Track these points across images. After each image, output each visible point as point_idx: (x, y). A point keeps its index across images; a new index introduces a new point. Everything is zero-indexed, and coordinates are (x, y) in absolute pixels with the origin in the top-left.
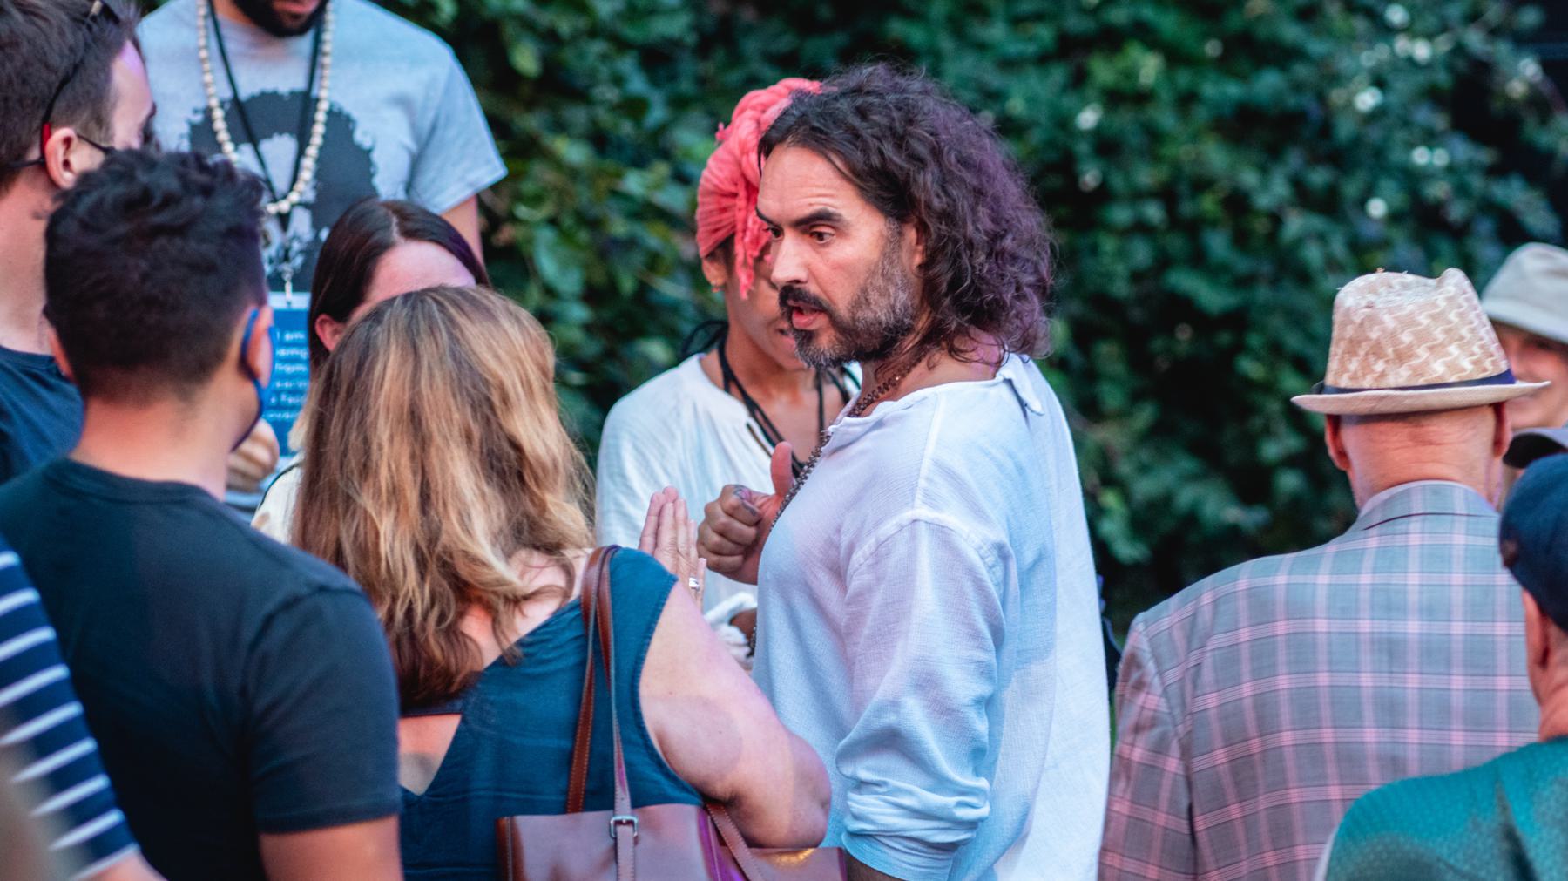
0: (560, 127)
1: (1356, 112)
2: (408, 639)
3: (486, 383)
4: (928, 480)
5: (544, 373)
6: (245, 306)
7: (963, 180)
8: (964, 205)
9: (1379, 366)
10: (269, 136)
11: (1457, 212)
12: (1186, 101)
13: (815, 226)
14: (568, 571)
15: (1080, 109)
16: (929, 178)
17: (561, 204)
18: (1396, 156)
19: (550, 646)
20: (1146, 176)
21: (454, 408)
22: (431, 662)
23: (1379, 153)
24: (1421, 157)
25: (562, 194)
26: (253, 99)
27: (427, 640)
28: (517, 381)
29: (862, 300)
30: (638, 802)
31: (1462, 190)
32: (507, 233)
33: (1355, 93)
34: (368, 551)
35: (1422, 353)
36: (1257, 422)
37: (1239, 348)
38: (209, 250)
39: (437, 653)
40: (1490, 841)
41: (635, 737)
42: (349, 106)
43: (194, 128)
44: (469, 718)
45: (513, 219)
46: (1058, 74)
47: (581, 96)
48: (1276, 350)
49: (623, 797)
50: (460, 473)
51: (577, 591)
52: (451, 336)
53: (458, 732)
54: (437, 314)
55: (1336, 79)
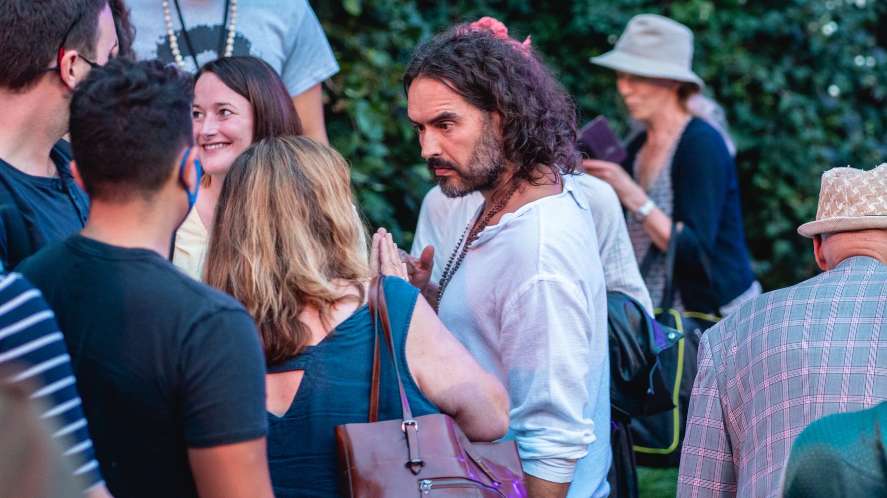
0: (371, 44)
1: (824, 36)
2: (270, 324)
3: (312, 184)
5: (345, 181)
6: (181, 149)
7: (520, 84)
8: (521, 98)
9: (840, 206)
10: (202, 52)
12: (726, 29)
14: (360, 287)
16: (500, 85)
17: (372, 88)
18: (845, 61)
19: (354, 330)
21: (294, 198)
22: (284, 339)
23: (836, 59)
24: (859, 61)
25: (372, 82)
26: (193, 30)
27: (282, 327)
28: (330, 187)
29: (475, 159)
30: (414, 415)
32: (341, 105)
33: (822, 25)
34: (245, 279)
35: (864, 199)
36: (765, 213)
37: (755, 170)
38: (163, 114)
39: (288, 334)
40: (870, 450)
41: (407, 380)
42: (247, 34)
43: (160, 47)
45: (345, 97)
47: (384, 26)
48: (776, 172)
49: (407, 414)
50: (299, 233)
51: (366, 300)
52: (292, 159)
54: (284, 148)
55: (812, 16)
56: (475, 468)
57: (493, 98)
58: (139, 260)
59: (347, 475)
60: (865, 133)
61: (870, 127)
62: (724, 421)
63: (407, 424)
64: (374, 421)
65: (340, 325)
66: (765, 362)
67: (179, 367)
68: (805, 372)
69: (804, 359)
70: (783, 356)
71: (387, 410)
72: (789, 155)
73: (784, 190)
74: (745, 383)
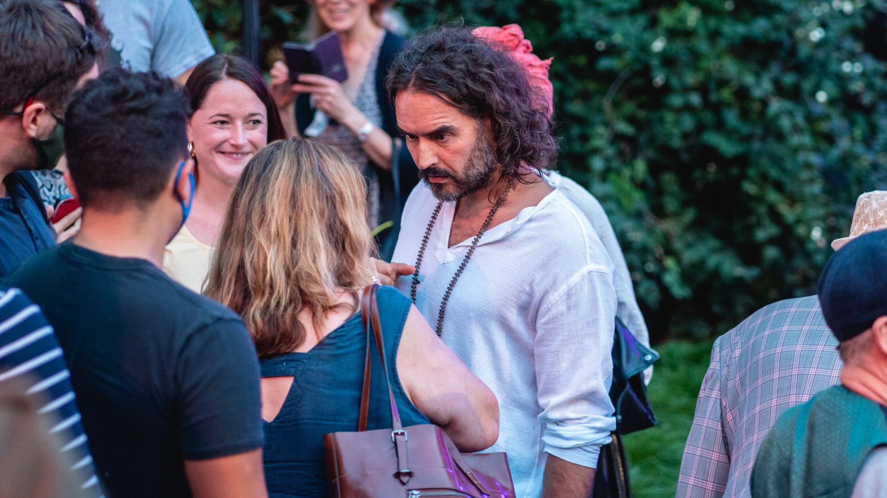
4: (591, 248)
6: (177, 160)
11: (867, 99)
12: (714, 35)
13: (438, 135)
14: (354, 295)
15: (654, 39)
18: (833, 67)
20: (691, 78)
23: (823, 65)
29: (470, 164)
30: (405, 424)
31: (870, 86)
33: (810, 31)
36: (753, 219)
37: (743, 176)
38: (159, 124)
41: (398, 391)
44: (298, 379)
46: (642, 20)
48: (764, 177)
51: (359, 309)
53: (292, 387)
55: (799, 23)
56: (464, 479)
57: (490, 107)
58: (132, 270)
59: (336, 483)
60: (853, 139)
61: (858, 133)
62: (722, 423)
63: (396, 434)
64: (363, 430)
65: (331, 333)
66: (760, 362)
67: (175, 378)
68: (795, 372)
69: (796, 360)
70: (777, 357)
71: (374, 418)
72: (777, 161)
73: (773, 196)
74: (742, 384)
